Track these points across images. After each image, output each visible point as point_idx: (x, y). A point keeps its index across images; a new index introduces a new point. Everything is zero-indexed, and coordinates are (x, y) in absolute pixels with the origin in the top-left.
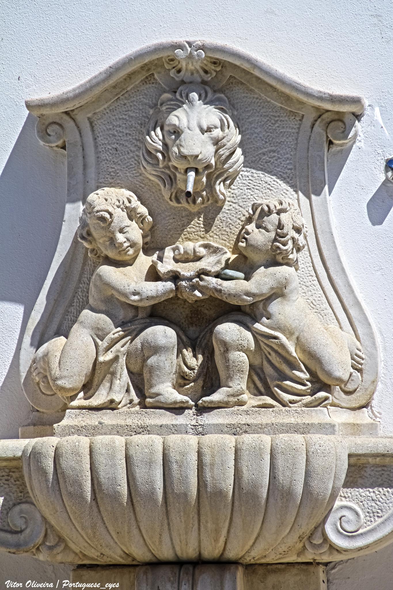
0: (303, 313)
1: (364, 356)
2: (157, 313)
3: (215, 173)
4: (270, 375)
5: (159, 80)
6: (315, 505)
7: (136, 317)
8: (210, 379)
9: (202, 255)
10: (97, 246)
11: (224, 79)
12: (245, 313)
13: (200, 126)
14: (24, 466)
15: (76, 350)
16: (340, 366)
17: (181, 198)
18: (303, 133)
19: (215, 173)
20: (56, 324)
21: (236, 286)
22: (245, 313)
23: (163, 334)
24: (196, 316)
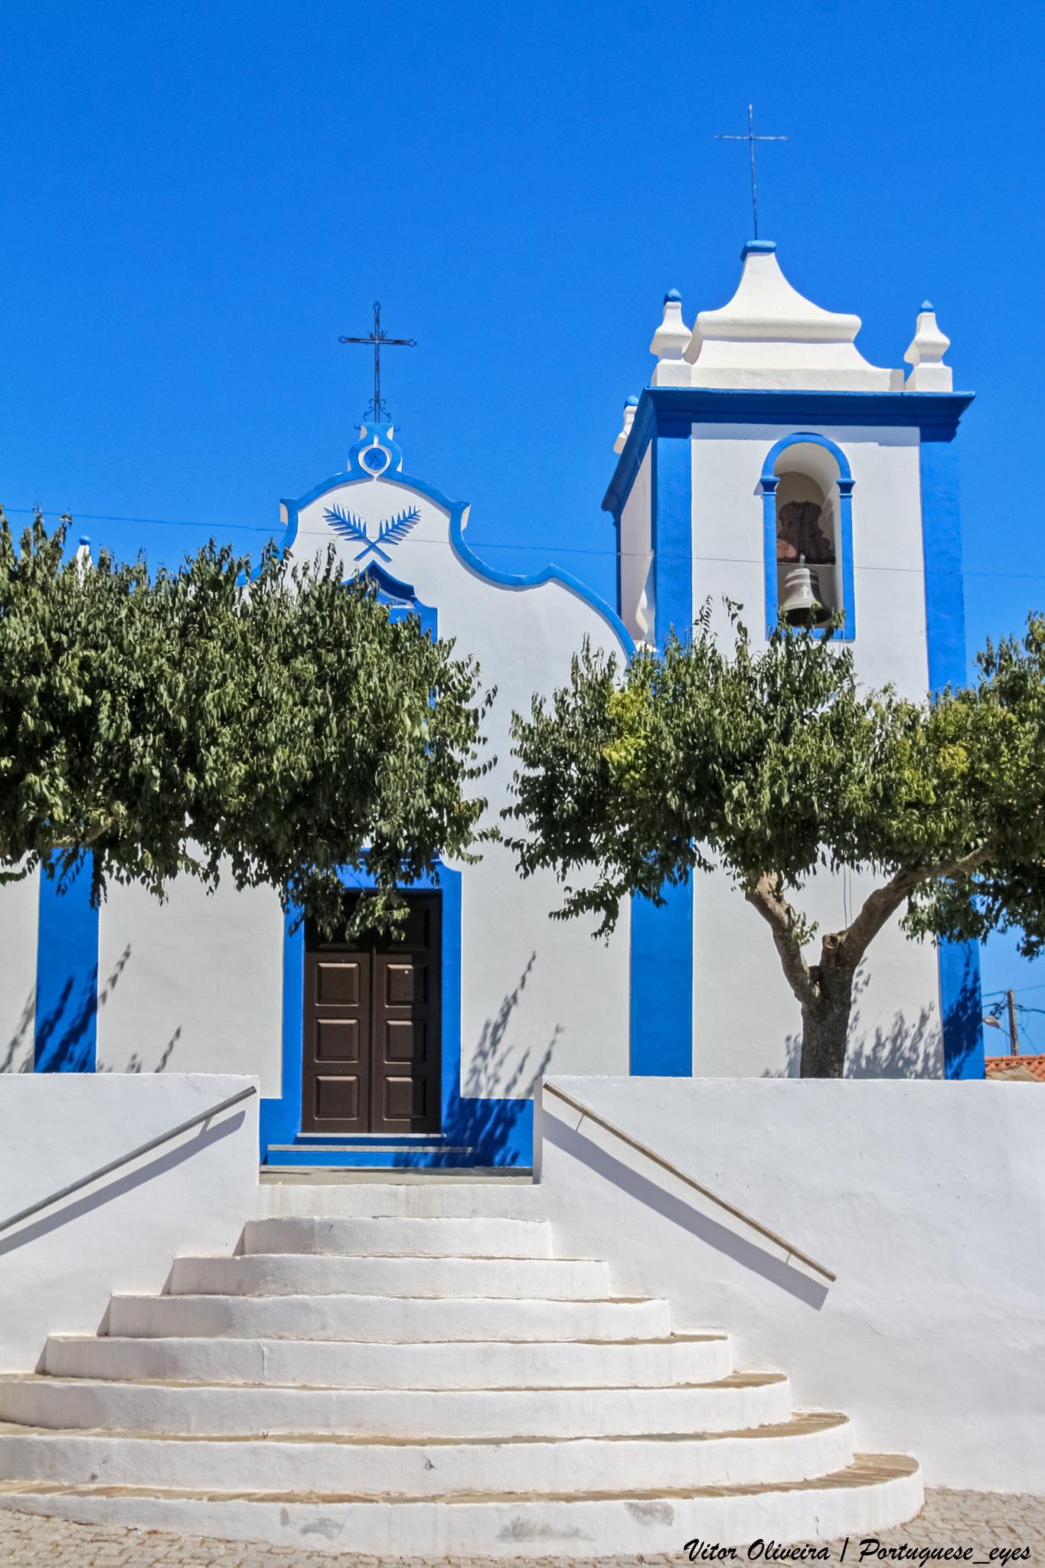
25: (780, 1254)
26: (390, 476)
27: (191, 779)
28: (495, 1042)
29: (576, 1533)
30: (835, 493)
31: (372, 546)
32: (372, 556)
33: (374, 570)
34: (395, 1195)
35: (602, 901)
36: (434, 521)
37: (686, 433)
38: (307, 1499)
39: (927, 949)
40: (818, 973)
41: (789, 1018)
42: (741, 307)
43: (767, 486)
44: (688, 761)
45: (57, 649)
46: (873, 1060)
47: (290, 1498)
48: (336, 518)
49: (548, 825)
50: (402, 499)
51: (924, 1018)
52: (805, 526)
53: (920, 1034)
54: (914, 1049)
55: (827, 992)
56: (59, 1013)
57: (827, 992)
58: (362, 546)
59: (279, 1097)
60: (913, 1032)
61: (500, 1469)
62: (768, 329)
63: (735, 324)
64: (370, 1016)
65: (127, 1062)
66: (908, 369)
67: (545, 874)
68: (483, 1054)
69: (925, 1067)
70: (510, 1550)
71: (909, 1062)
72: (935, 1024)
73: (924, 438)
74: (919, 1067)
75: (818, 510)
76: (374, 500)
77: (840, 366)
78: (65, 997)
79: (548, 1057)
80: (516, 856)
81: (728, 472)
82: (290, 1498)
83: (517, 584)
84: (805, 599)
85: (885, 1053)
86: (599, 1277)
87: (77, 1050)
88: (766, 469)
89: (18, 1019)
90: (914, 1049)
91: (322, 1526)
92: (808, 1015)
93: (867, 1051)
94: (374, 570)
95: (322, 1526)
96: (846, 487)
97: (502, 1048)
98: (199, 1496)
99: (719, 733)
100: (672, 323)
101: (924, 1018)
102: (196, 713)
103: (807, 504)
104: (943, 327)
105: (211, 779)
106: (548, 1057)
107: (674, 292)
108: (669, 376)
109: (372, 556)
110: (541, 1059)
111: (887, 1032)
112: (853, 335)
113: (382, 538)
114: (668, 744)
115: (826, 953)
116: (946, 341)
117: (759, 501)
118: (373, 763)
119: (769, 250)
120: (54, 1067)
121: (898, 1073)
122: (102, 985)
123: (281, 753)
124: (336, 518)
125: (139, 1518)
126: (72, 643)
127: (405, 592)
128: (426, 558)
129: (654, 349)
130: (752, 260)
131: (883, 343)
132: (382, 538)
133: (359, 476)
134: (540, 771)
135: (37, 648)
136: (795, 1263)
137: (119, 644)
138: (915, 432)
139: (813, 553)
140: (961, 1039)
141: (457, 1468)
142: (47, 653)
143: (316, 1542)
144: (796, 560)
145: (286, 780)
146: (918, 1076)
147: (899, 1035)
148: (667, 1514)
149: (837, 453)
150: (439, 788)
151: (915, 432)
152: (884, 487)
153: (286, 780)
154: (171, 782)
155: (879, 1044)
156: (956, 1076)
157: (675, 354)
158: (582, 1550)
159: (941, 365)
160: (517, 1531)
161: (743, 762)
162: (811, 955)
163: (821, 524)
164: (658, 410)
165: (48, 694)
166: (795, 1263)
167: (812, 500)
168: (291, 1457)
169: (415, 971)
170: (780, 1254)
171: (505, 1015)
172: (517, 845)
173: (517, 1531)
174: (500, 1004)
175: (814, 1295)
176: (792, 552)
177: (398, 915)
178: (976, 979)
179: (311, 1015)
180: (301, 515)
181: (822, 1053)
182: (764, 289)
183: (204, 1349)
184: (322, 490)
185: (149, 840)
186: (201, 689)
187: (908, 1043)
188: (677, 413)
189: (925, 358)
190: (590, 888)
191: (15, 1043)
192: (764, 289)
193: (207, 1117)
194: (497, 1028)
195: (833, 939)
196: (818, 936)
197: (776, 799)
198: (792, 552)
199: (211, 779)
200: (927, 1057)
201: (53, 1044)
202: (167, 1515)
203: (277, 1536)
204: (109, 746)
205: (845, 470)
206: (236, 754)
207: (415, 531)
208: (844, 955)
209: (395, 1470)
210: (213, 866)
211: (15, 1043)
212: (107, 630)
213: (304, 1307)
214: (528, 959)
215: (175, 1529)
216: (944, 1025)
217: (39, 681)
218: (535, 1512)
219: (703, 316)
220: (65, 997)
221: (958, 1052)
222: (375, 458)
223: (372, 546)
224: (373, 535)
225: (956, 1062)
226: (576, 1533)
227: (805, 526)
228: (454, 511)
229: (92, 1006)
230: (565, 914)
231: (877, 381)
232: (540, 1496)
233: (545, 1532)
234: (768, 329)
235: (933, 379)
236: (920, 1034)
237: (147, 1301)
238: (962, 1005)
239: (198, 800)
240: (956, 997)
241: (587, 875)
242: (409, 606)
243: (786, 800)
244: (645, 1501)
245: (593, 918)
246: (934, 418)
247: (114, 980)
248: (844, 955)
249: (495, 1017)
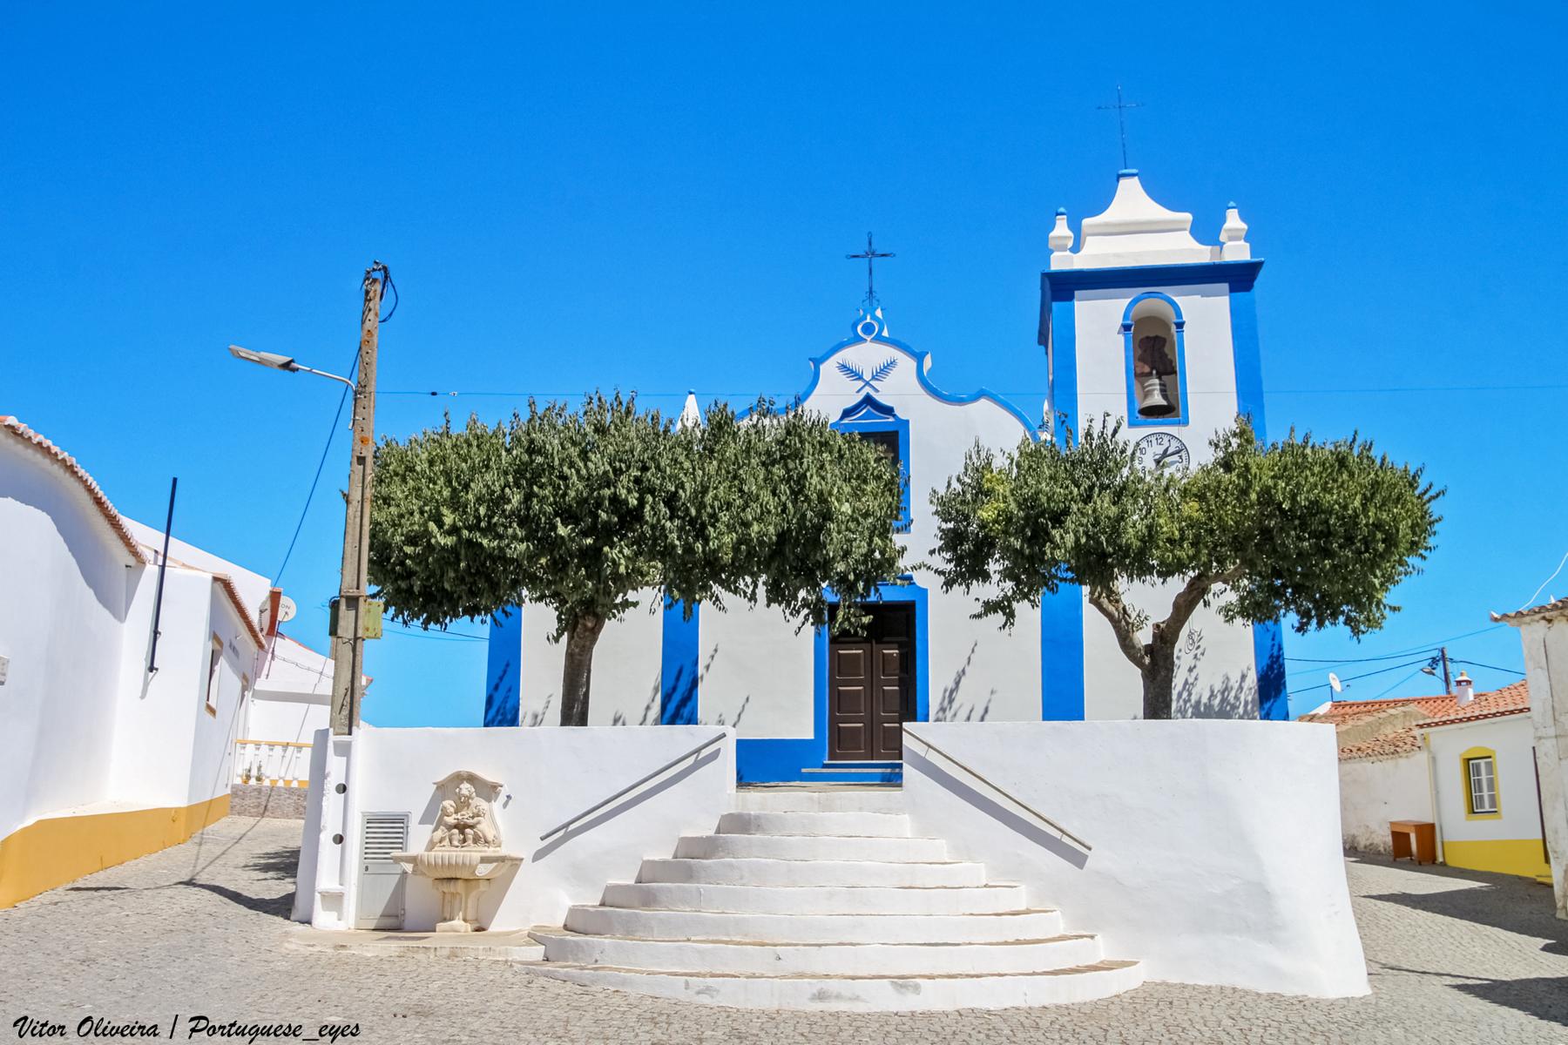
0: (485, 827)
1: (1101, 950)
2: (456, 827)
3: (469, 798)
4: (476, 840)
5: (459, 778)
6: (473, 868)
7: (450, 827)
8: (464, 841)
9: (465, 816)
10: (445, 813)
11: (471, 779)
12: (472, 827)
13: (466, 788)
14: (328, 852)
15: (439, 834)
16: (490, 838)
17: (463, 803)
18: (489, 790)
19: (469, 798)
20: (436, 829)
21: (471, 821)
22: (472, 827)
23: (456, 831)
24: (461, 827)
25: (1057, 834)
26: (879, 339)
27: (699, 546)
28: (951, 701)
29: (857, 998)
30: (1174, 328)
31: (867, 383)
32: (867, 390)
33: (868, 400)
34: (811, 799)
35: (1002, 607)
36: (906, 364)
37: (1071, 298)
38: (697, 975)
39: (1244, 631)
40: (1149, 649)
41: (1132, 680)
42: (1115, 213)
43: (1126, 328)
44: (1027, 518)
45: (618, 472)
46: (1209, 707)
47: (691, 975)
48: (844, 368)
49: (959, 560)
50: (887, 353)
51: (1243, 677)
52: (1154, 352)
53: (1241, 688)
54: (1237, 698)
55: (1156, 663)
56: (674, 689)
57: (1156, 663)
58: (861, 384)
59: (811, 736)
60: (1236, 686)
61: (820, 961)
62: (1135, 225)
63: (1107, 225)
64: (871, 684)
65: (716, 718)
66: (1222, 245)
67: (958, 589)
68: (943, 710)
69: (1245, 711)
70: (818, 1006)
71: (1234, 707)
72: (1252, 680)
73: (1232, 290)
74: (1241, 710)
75: (1164, 340)
76: (867, 355)
77: (1183, 249)
78: (678, 679)
79: (986, 711)
80: (942, 579)
81: (1099, 324)
82: (691, 975)
83: (961, 402)
84: (1157, 399)
85: (1217, 702)
86: (940, 848)
87: (686, 712)
88: (1125, 317)
89: (650, 693)
90: (1237, 698)
91: (707, 990)
92: (1145, 677)
93: (1204, 700)
94: (868, 400)
95: (707, 990)
96: (1180, 325)
97: (955, 705)
98: (642, 972)
99: (1044, 499)
100: (1061, 229)
101: (1243, 677)
102: (701, 506)
103: (1157, 337)
104: (1243, 218)
105: (713, 545)
106: (986, 711)
107: (1062, 210)
108: (1061, 262)
109: (867, 390)
110: (981, 712)
111: (1218, 687)
112: (1188, 226)
113: (873, 378)
114: (1013, 506)
115: (1154, 635)
116: (1245, 227)
117: (1121, 338)
118: (819, 528)
119: (1133, 175)
120: (672, 721)
121: (1227, 716)
122: (701, 670)
123: (756, 527)
124: (844, 368)
125: (610, 984)
126: (628, 468)
127: (889, 411)
128: (902, 390)
129: (1051, 245)
130: (1123, 182)
131: (1206, 231)
132: (873, 378)
133: (858, 340)
134: (951, 525)
135: (605, 473)
136: (1066, 840)
137: (658, 468)
138: (1226, 286)
139: (1161, 369)
140: (1271, 688)
141: (795, 960)
142: (611, 475)
143: (705, 999)
144: (1150, 374)
145: (761, 543)
146: (1241, 718)
147: (1226, 689)
148: (917, 988)
149: (1173, 304)
150: (876, 540)
151: (1226, 286)
152: (1205, 322)
153: (761, 543)
154: (689, 549)
155: (1212, 695)
156: (1267, 717)
157: (1063, 248)
158: (860, 1008)
159: (1242, 242)
160: (821, 996)
161: (1058, 518)
162: (1144, 637)
163: (1167, 350)
164: (1052, 285)
165: (615, 499)
166: (1066, 840)
167: (1160, 334)
168: (699, 952)
169: (901, 654)
170: (1057, 834)
171: (957, 683)
172: (942, 573)
173: (821, 996)
174: (954, 676)
175: (1079, 860)
176: (1147, 369)
177: (866, 620)
178: (1280, 648)
179: (833, 684)
180: (822, 367)
181: (1157, 705)
182: (1132, 199)
183: (670, 890)
184: (834, 350)
185: (691, 578)
186: (705, 491)
187: (1233, 694)
188: (1064, 286)
189: (1231, 239)
190: (993, 598)
191: (648, 708)
192: (1132, 199)
193: (698, 751)
194: (952, 692)
195: (1157, 626)
196: (1150, 623)
197: (1077, 540)
198: (1147, 369)
199: (713, 545)
200: (1246, 703)
201: (671, 707)
202: (624, 982)
203: (683, 996)
204: (653, 527)
205: (1179, 315)
206: (731, 528)
207: (894, 373)
208: (1166, 636)
209: (759, 960)
210: (754, 592)
211: (648, 708)
212: (652, 458)
213: (731, 866)
214: (973, 643)
215: (628, 990)
216: (1259, 680)
217: (607, 492)
218: (832, 985)
219: (1086, 222)
220: (678, 679)
221: (1268, 699)
222: (868, 329)
223: (867, 383)
224: (867, 377)
225: (1267, 706)
226: (857, 998)
227: (1154, 352)
228: (919, 358)
229: (694, 683)
230: (979, 616)
231: (1201, 255)
232: (836, 976)
233: (838, 997)
234: (1135, 225)
235: (1237, 251)
236: (1241, 688)
237: (664, 863)
238: (1270, 667)
239: (1124, 487)
240: (1266, 661)
241: (993, 589)
242: (891, 419)
243: (1083, 540)
244: (902, 982)
245: (1000, 617)
246: (1239, 277)
247: (708, 667)
248: (1166, 636)
249: (951, 685)
